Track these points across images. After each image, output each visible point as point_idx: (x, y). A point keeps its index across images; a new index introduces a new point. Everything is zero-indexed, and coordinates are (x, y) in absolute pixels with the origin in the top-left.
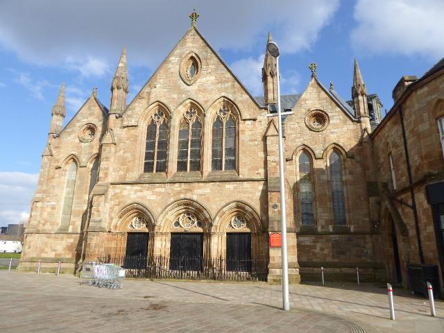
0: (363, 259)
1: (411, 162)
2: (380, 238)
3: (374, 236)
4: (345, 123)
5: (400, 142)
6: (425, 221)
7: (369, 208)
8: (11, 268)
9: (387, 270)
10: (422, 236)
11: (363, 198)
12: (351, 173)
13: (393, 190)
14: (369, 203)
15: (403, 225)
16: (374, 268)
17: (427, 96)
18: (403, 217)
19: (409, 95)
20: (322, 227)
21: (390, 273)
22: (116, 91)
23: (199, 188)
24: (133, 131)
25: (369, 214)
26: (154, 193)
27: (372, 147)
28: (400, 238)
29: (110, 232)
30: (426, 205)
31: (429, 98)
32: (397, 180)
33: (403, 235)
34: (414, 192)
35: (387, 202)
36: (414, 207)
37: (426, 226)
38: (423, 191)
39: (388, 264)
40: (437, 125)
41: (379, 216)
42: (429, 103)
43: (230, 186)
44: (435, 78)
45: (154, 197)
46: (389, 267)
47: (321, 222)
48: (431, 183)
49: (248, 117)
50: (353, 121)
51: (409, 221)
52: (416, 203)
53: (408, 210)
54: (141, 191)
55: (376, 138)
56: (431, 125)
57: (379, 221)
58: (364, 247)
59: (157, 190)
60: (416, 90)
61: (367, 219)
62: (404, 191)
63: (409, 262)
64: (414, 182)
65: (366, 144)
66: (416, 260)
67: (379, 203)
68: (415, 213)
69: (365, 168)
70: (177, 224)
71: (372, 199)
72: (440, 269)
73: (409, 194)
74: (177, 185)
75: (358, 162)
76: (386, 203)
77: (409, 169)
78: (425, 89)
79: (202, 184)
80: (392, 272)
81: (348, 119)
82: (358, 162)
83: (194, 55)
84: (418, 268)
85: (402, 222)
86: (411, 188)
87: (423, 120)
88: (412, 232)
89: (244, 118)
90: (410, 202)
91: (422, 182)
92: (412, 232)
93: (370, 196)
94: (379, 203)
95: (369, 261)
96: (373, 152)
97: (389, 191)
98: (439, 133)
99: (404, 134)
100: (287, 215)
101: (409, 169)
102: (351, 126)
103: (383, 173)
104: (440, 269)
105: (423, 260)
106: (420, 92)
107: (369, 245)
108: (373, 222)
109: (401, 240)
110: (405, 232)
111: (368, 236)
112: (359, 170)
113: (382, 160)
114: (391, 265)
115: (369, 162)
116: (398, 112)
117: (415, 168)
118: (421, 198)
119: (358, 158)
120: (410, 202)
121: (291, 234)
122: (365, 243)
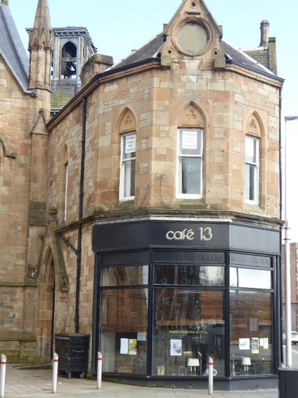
0: (6, 326)
1: (85, 187)
2: (37, 294)
3: (28, 290)
4: (10, 92)
5: (78, 151)
6: (87, 274)
7: (27, 246)
8: (103, 380)
9: (39, 342)
10: (81, 294)
11: (19, 228)
13: (64, 221)
14: (28, 236)
15: (65, 277)
16: (20, 341)
17: (115, 98)
18: (66, 264)
19: (96, 88)
21: (41, 348)
22: (267, 105)
24: (146, 121)
25: (25, 255)
27: (47, 144)
28: (58, 295)
30: (91, 253)
32: (69, 214)
33: (63, 292)
34: (83, 230)
36: (78, 252)
37: (87, 280)
38: (91, 231)
39: (41, 334)
40: (119, 143)
41: (40, 261)
42: (115, 108)
44: (127, 76)
46: (41, 339)
48: (100, 223)
50: (25, 94)
51: (71, 271)
52: (82, 247)
53: (73, 255)
55: (54, 131)
56: (112, 142)
57: (39, 267)
58: (11, 307)
61: (21, 262)
62: (72, 227)
63: (65, 329)
64: (85, 216)
65: (39, 138)
66: (71, 330)
67: (42, 238)
68: (79, 261)
69: (31, 177)
71: (34, 231)
72: (91, 339)
73: (77, 232)
75: (21, 165)
76: (50, 241)
77: (82, 196)
78: (114, 87)
80: (44, 347)
81: (16, 88)
82: (21, 165)
84: (66, 338)
85: (65, 272)
86: (78, 226)
87: (105, 132)
88: (72, 288)
90: (76, 246)
91: (91, 219)
92: (72, 288)
93: (32, 225)
95: (15, 329)
96: (46, 153)
97: (57, 222)
98: (119, 155)
99: (83, 142)
100: (155, 276)
101: (82, 196)
102: (17, 101)
103: (55, 192)
104: (91, 339)
105: (77, 329)
107: (18, 305)
108: (29, 268)
109: (59, 299)
110: (65, 285)
111: (18, 290)
112: (20, 179)
113: (56, 170)
114: (44, 336)
115: (39, 168)
116: (82, 104)
117: (87, 196)
118: (87, 240)
119: (22, 158)
120: (76, 246)
122: (13, 300)
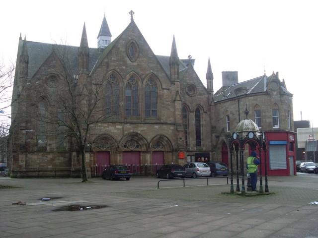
12: (205, 121)
20: (192, 148)
23: (141, 127)
25: (212, 142)
26: (115, 128)
29: (173, 151)
31: (253, 102)
35: (224, 138)
43: (157, 127)
45: (116, 131)
47: (191, 145)
49: (165, 88)
54: (108, 127)
55: (218, 105)
59: (117, 127)
60: (248, 96)
70: (125, 146)
71: (214, 135)
74: (128, 125)
78: (252, 98)
79: (142, 125)
83: (134, 42)
89: (163, 87)
94: (218, 137)
106: (250, 98)
112: (208, 119)
121: (304, 144)
